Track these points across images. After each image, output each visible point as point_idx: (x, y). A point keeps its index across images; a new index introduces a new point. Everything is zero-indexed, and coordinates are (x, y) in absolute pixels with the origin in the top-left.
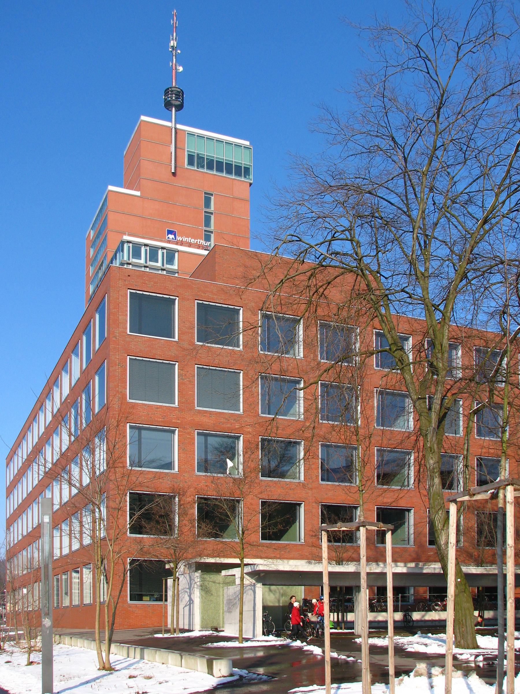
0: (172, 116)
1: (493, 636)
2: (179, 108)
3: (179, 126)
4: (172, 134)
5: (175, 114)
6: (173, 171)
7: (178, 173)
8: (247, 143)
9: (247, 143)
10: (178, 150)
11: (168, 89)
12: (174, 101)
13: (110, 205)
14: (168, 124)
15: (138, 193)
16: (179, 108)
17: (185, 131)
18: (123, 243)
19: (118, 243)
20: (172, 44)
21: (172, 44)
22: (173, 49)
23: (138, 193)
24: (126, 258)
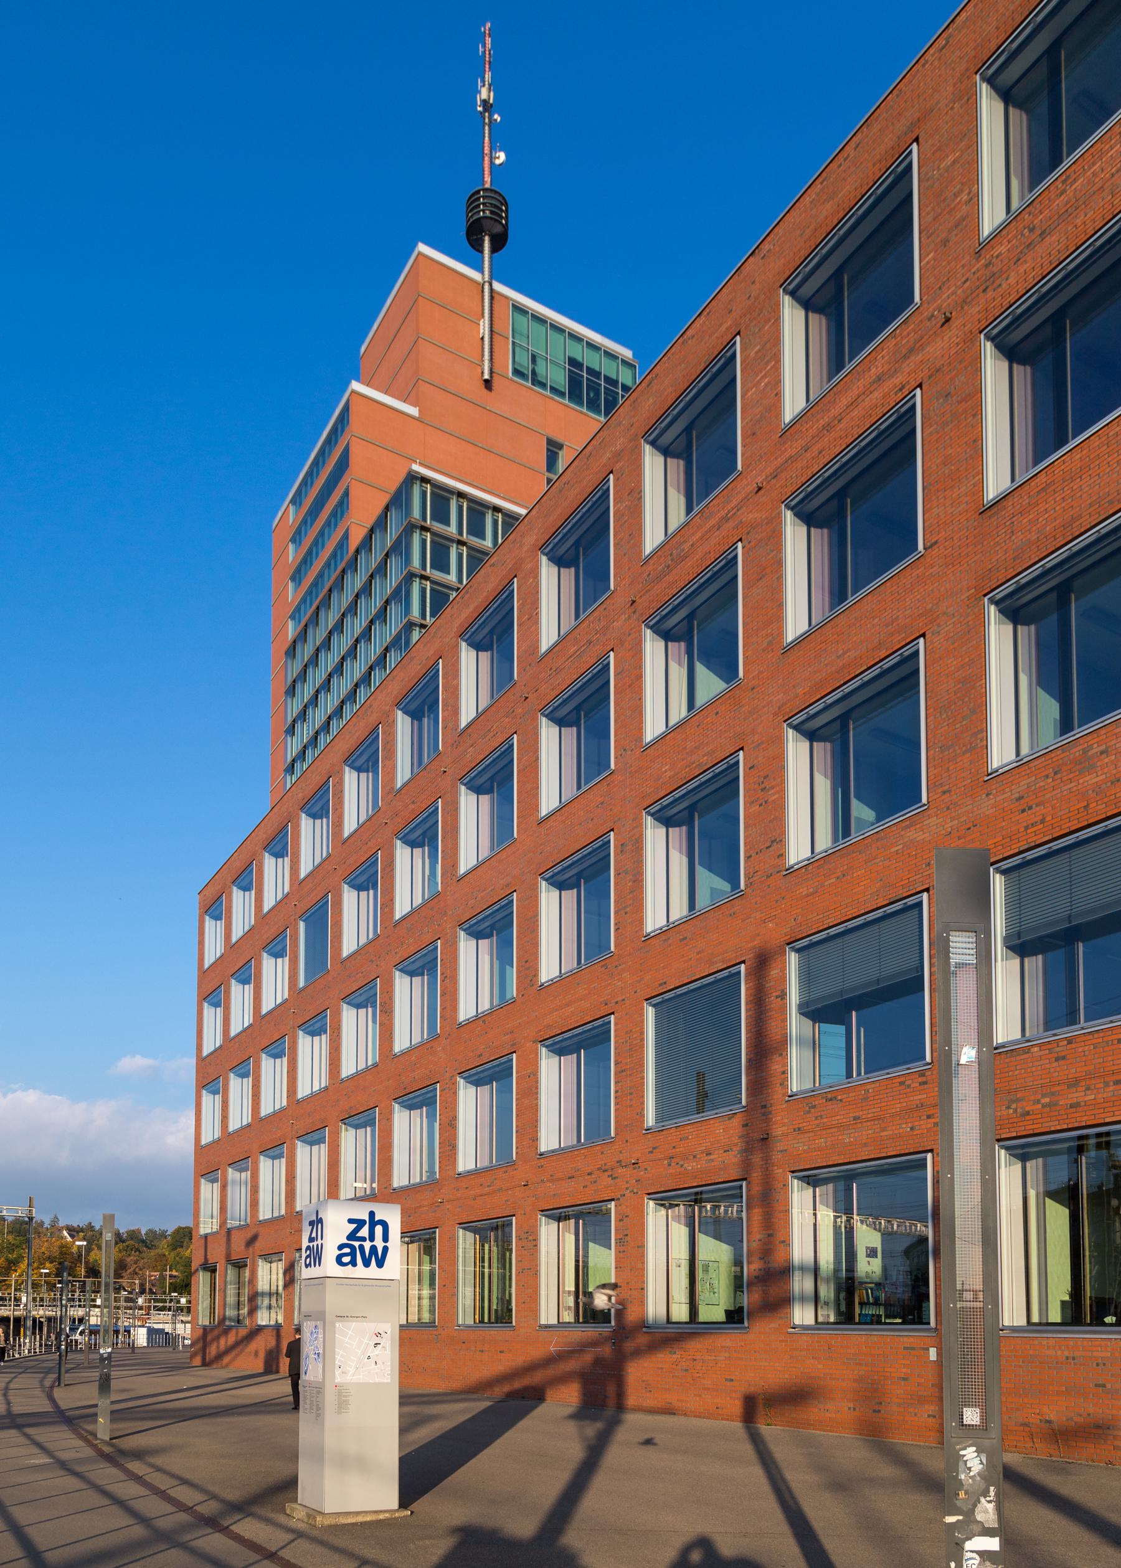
0: (483, 261)
1: (133, 1235)
2: (499, 242)
3: (498, 286)
4: (483, 296)
5: (491, 258)
6: (486, 376)
7: (496, 384)
8: (627, 353)
9: (627, 353)
10: (495, 337)
11: (478, 192)
12: (485, 228)
13: (356, 424)
14: (475, 275)
15: (414, 411)
16: (499, 242)
17: (507, 298)
18: (413, 478)
19: (401, 476)
20: (484, 93)
21: (484, 93)
22: (485, 110)
23: (414, 411)
24: (416, 513)
